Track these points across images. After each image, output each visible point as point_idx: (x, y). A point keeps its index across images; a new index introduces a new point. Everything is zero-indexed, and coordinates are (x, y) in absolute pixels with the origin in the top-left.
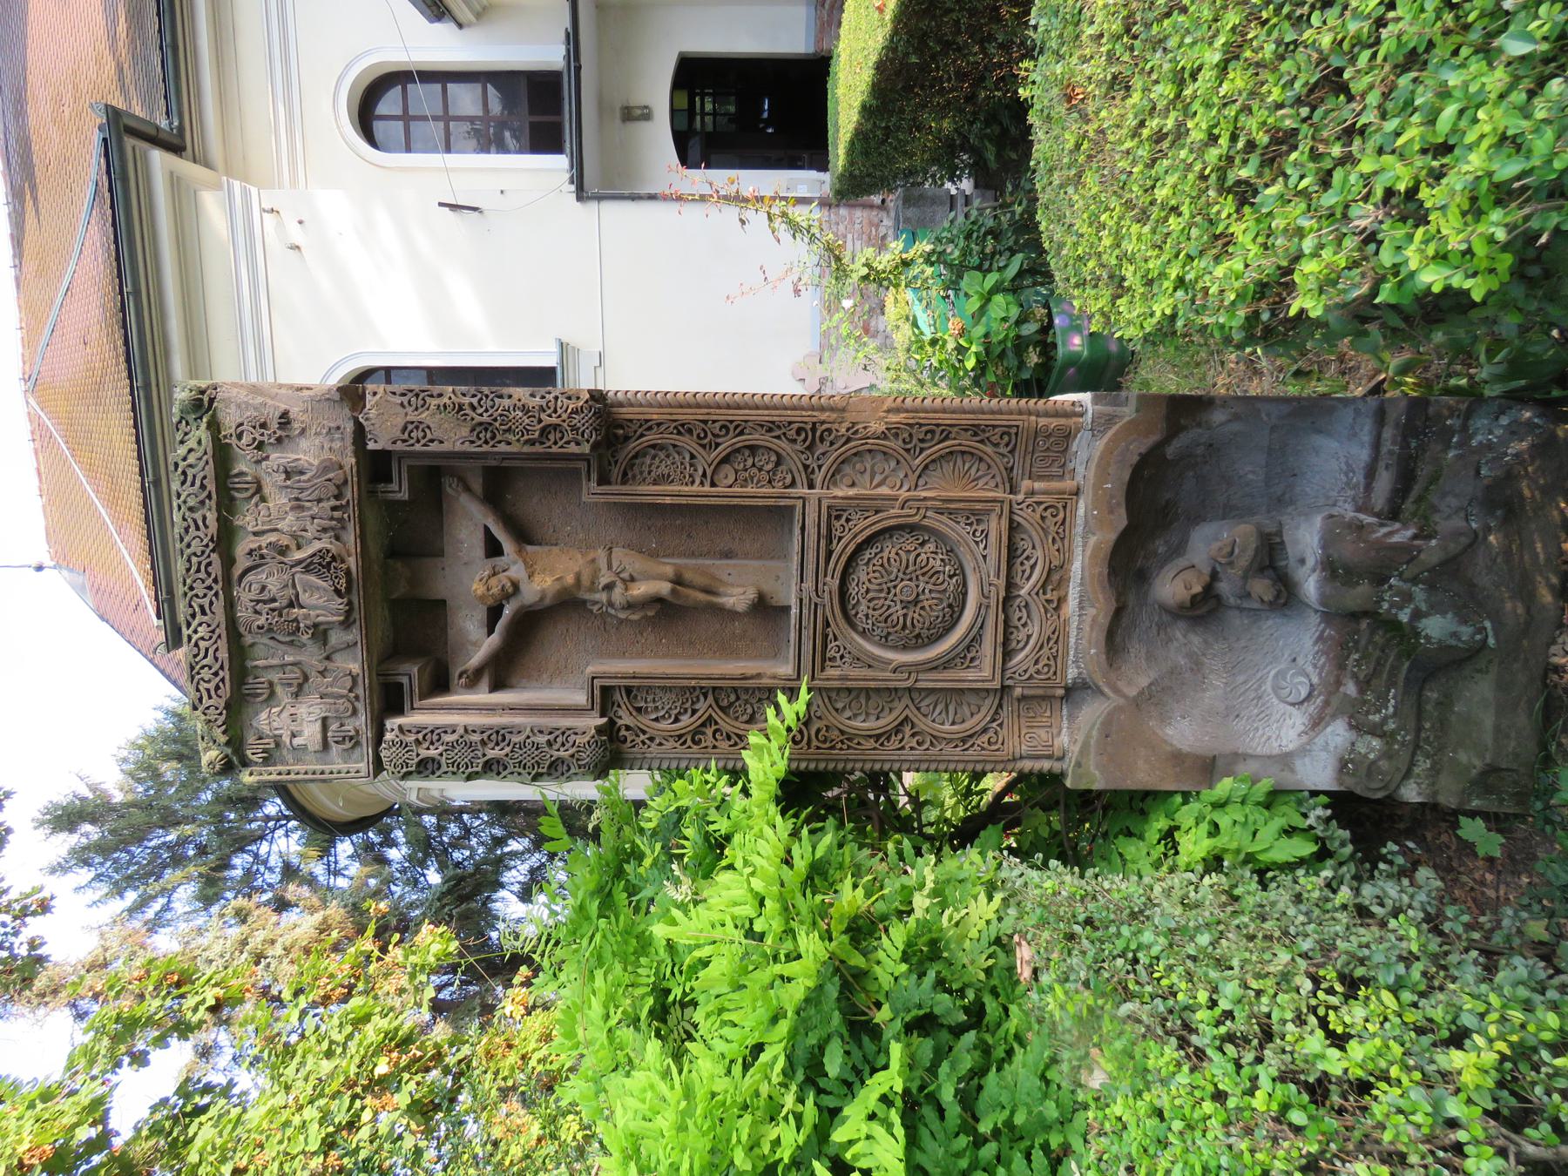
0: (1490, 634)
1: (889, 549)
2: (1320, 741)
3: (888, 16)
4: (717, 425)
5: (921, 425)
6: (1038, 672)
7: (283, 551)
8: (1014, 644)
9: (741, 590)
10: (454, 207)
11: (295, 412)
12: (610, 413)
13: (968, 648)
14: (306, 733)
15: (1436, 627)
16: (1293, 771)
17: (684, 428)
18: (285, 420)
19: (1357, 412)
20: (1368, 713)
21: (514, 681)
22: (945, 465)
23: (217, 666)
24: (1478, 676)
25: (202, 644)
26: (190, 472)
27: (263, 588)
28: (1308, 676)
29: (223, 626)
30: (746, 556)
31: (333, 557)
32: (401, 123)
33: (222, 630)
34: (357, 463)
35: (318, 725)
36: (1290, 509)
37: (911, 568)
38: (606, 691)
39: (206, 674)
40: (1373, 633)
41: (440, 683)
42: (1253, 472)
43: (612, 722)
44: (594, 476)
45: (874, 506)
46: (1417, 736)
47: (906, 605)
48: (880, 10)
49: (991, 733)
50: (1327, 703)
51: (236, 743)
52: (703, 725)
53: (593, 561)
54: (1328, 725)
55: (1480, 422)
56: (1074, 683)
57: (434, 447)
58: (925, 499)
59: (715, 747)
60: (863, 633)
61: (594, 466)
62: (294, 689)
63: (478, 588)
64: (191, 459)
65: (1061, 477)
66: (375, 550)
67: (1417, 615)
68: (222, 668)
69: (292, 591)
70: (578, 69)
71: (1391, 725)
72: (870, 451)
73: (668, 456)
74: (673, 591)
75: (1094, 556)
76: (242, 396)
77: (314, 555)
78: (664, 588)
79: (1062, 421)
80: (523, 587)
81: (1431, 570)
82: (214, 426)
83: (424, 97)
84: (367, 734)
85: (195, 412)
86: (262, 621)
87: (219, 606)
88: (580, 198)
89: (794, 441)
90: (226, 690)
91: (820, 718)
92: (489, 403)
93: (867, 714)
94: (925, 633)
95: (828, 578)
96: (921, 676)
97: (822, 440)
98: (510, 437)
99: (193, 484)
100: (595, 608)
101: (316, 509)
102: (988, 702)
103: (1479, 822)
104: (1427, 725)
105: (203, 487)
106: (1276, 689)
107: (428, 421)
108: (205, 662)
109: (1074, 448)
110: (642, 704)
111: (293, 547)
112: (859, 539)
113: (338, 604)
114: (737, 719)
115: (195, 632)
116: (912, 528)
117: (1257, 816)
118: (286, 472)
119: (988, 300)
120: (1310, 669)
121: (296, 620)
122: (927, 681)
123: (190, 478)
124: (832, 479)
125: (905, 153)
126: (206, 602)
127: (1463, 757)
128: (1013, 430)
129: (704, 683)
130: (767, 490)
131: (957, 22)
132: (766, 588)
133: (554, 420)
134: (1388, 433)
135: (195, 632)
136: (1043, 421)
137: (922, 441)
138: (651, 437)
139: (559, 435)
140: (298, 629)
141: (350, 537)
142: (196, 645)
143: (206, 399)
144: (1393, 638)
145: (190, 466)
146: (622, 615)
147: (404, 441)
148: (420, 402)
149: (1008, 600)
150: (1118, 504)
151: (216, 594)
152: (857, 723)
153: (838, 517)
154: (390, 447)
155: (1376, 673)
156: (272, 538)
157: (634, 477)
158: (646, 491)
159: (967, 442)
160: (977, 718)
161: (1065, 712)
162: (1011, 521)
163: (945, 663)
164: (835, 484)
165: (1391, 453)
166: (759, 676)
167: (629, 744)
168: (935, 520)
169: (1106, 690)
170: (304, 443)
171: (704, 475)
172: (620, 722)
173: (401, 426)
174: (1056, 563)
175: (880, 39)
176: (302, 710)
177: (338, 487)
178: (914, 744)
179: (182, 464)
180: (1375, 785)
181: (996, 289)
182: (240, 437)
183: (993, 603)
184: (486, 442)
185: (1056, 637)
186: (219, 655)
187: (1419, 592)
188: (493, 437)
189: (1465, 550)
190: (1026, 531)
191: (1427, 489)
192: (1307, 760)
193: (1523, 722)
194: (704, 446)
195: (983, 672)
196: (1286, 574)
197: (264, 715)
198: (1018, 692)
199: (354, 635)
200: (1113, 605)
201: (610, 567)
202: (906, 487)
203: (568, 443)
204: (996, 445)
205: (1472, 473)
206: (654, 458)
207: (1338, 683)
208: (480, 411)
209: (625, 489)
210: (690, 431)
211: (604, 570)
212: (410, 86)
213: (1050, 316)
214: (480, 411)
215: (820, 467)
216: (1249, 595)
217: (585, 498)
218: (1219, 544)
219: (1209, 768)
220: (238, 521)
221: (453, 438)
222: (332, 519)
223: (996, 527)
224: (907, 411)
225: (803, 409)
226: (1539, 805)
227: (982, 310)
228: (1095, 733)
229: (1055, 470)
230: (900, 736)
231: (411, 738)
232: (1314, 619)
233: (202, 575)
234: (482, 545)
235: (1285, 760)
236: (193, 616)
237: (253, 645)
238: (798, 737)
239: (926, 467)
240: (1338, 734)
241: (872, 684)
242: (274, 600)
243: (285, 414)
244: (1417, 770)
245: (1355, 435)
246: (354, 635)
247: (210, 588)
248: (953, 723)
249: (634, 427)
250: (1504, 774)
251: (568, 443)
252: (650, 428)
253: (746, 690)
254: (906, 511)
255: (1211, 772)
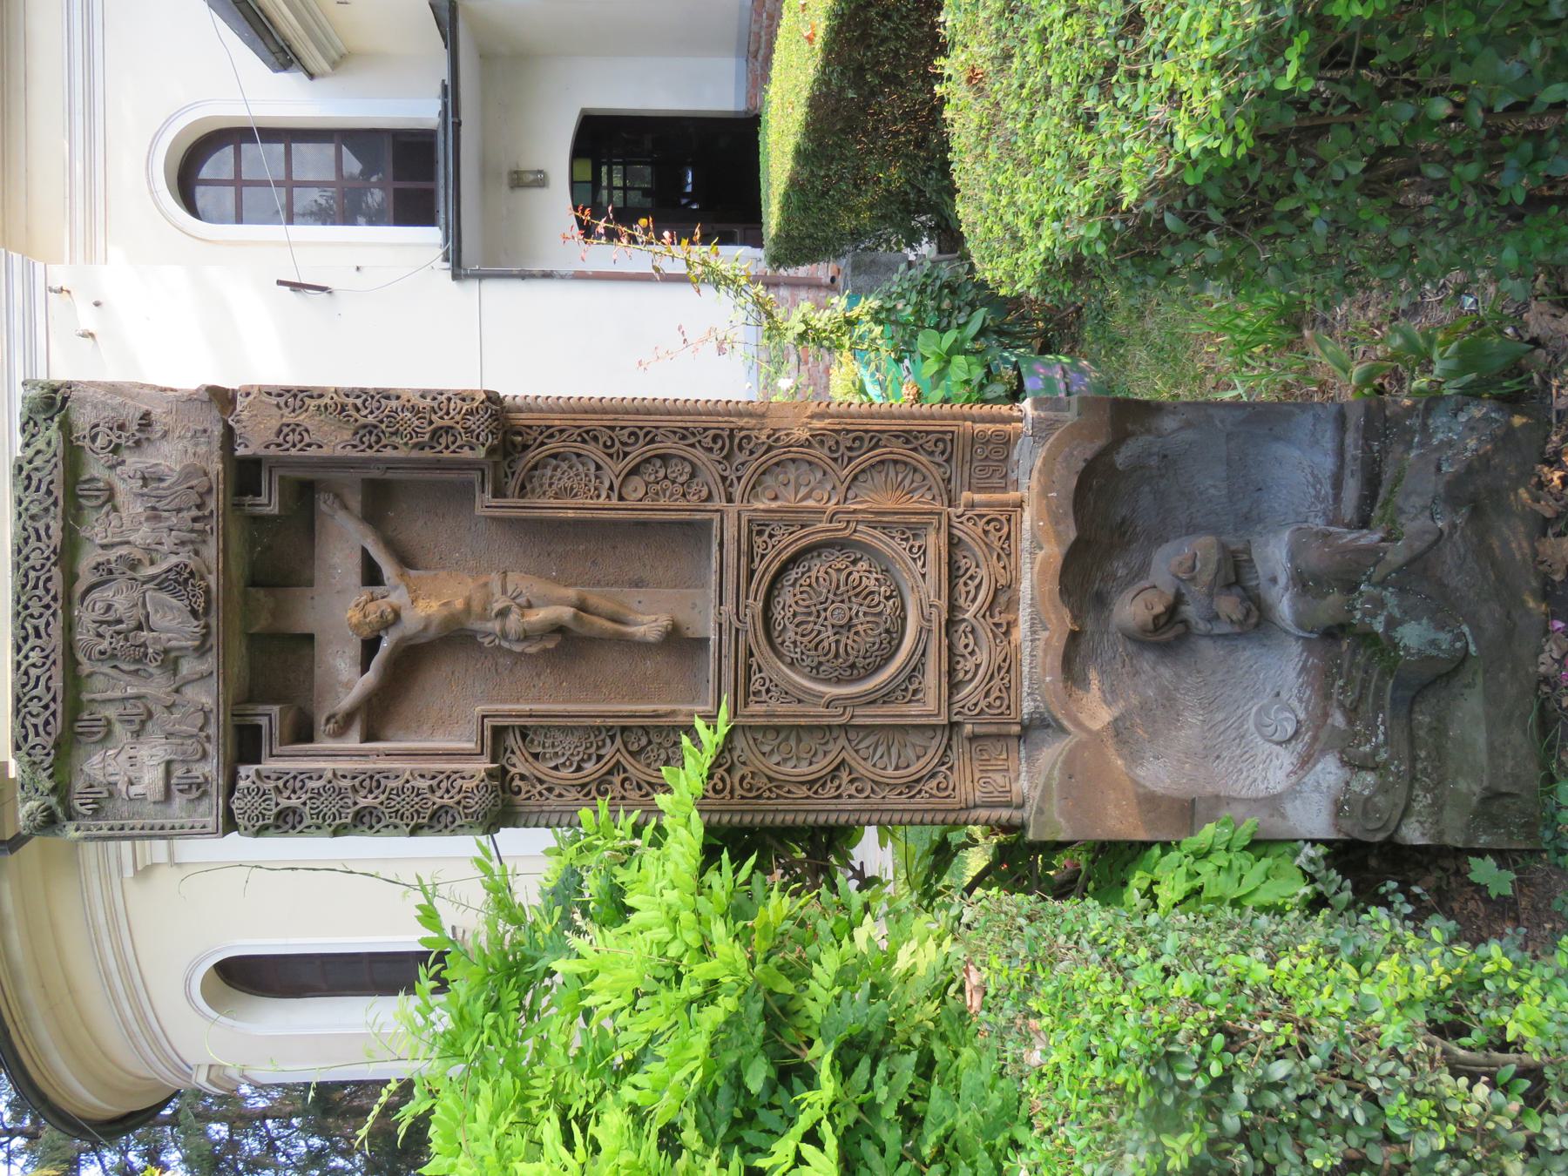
0: (1470, 639)
1: (818, 567)
2: (1310, 780)
3: (818, 43)
4: (626, 432)
5: (848, 431)
6: (989, 706)
7: (134, 565)
8: (961, 675)
9: (653, 617)
10: (296, 287)
11: (157, 412)
12: (507, 419)
13: (910, 678)
14: (146, 780)
15: (1413, 635)
16: (1283, 816)
17: (587, 435)
18: (146, 421)
19: (1317, 418)
20: (1359, 745)
21: (389, 733)
22: (876, 475)
23: (47, 698)
24: (1466, 691)
25: (33, 672)
26: (35, 477)
27: (109, 608)
28: (1293, 711)
29: (59, 650)
30: (659, 585)
31: (192, 574)
32: (232, 189)
33: (58, 656)
34: (224, 469)
35: (161, 769)
36: (1259, 528)
37: (842, 588)
38: (499, 733)
39: (35, 707)
40: (1354, 654)
41: (303, 732)
42: (1215, 486)
43: (504, 771)
44: (489, 487)
45: (797, 519)
46: (1413, 767)
47: (838, 630)
48: (810, 39)
49: (940, 778)
50: (1315, 738)
51: (61, 790)
52: (610, 772)
53: (486, 585)
54: (1317, 761)
55: (1439, 421)
56: (1031, 720)
57: (312, 452)
58: (855, 511)
59: (623, 798)
60: (791, 665)
61: (489, 474)
62: (135, 727)
63: (354, 615)
64: (38, 462)
65: (1004, 489)
66: (237, 571)
67: (1392, 623)
68: (54, 699)
69: (141, 611)
70: (457, 125)
71: (1383, 756)
72: (793, 460)
73: (571, 467)
74: (576, 616)
75: (1042, 572)
76: (100, 395)
77: (170, 570)
78: (565, 613)
79: (1000, 426)
80: (404, 614)
81: (1399, 570)
82: (66, 427)
83: (263, 159)
84: (218, 781)
85: (45, 411)
86: (104, 645)
87: (56, 629)
88: (457, 275)
89: (710, 450)
90: (57, 726)
91: (744, 763)
92: (375, 404)
93: (798, 759)
94: (860, 662)
95: (751, 601)
96: (858, 711)
97: (741, 448)
98: (397, 440)
99: (38, 489)
100: (487, 641)
101: (175, 520)
102: (935, 742)
103: (1490, 861)
104: (1423, 754)
105: (49, 492)
106: (1260, 726)
107: (307, 423)
108: (34, 693)
109: (1015, 456)
110: (539, 750)
111: (147, 562)
112: (784, 556)
113: (194, 626)
114: (649, 765)
115: (26, 657)
116: (841, 545)
117: (1243, 861)
118: (144, 478)
119: (948, 362)
120: (1295, 703)
121: (144, 645)
122: (865, 716)
123: (34, 483)
124: (754, 489)
125: (851, 209)
126: (41, 623)
127: (1463, 785)
128: (949, 437)
129: (610, 722)
130: (682, 503)
131: (896, 51)
132: (682, 617)
133: (447, 422)
134: (1351, 438)
135: (26, 657)
136: (979, 427)
137: (850, 449)
138: (553, 446)
139: (451, 439)
140: (146, 655)
141: (211, 551)
142: (26, 673)
143: (59, 398)
144: (1374, 654)
145: (36, 469)
146: (517, 648)
147: (279, 445)
148: (298, 403)
149: (951, 623)
150: (1066, 514)
151: (54, 614)
152: (787, 768)
153: (760, 533)
154: (262, 452)
155: (1361, 698)
156: (123, 551)
157: (533, 490)
158: (545, 505)
159: (899, 450)
160: (923, 761)
161: (1023, 754)
162: (951, 536)
163: (885, 697)
164: (756, 497)
165: (1355, 458)
166: (673, 713)
167: (523, 796)
168: (865, 535)
169: (1066, 723)
170: (165, 447)
171: (611, 488)
172: (513, 771)
173: (275, 430)
174: (1002, 581)
175: (811, 71)
176: (143, 752)
177: (201, 495)
178: (853, 792)
179: (27, 467)
180: (1371, 826)
181: (957, 349)
182: (94, 439)
183: (935, 627)
184: (370, 447)
185: (1007, 666)
186: (51, 684)
187: (1389, 595)
188: (378, 441)
189: (1430, 547)
190: (970, 549)
191: (1392, 492)
192: (1298, 802)
193: (1520, 739)
194: (610, 456)
195: (929, 704)
196: (1258, 596)
197: (96, 759)
198: (968, 728)
199: (210, 663)
200: (1069, 625)
201: (504, 592)
202: (834, 501)
203: (461, 447)
204: (931, 453)
205: (1432, 469)
206: (555, 469)
207: (1326, 715)
208: (364, 412)
209: (522, 502)
210: (595, 439)
211: (498, 595)
212: (244, 146)
213: (1020, 378)
214: (364, 412)
215: (739, 479)
216: (1217, 617)
217: (479, 511)
218: (1179, 558)
219: (1188, 813)
220: (84, 532)
221: (334, 442)
222: (192, 531)
223: (934, 542)
224: (831, 416)
225: (719, 414)
226: (1548, 835)
227: (941, 374)
228: (1056, 773)
229: (995, 481)
230: (836, 783)
231: (270, 785)
232: (1295, 648)
233: (40, 592)
234: (359, 570)
235: (1273, 803)
236: (25, 639)
237: (90, 675)
238: (720, 786)
239: (855, 478)
240: (1329, 772)
241: (803, 721)
242: (120, 621)
243: (146, 415)
244: (1417, 806)
245: (1317, 442)
246: (210, 663)
247: (47, 607)
248: (897, 768)
249: (535, 434)
250: (1508, 801)
251: (461, 447)
252: (551, 436)
253: (659, 728)
254: (834, 525)
255: (1192, 817)
